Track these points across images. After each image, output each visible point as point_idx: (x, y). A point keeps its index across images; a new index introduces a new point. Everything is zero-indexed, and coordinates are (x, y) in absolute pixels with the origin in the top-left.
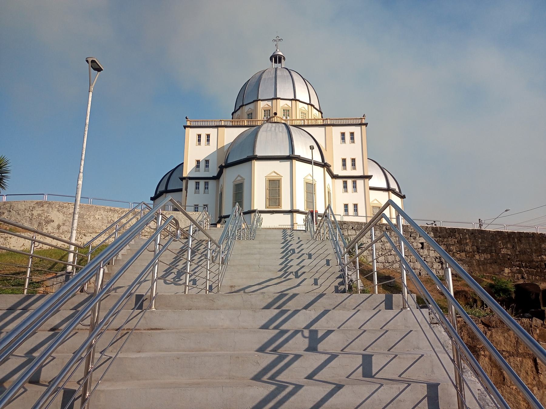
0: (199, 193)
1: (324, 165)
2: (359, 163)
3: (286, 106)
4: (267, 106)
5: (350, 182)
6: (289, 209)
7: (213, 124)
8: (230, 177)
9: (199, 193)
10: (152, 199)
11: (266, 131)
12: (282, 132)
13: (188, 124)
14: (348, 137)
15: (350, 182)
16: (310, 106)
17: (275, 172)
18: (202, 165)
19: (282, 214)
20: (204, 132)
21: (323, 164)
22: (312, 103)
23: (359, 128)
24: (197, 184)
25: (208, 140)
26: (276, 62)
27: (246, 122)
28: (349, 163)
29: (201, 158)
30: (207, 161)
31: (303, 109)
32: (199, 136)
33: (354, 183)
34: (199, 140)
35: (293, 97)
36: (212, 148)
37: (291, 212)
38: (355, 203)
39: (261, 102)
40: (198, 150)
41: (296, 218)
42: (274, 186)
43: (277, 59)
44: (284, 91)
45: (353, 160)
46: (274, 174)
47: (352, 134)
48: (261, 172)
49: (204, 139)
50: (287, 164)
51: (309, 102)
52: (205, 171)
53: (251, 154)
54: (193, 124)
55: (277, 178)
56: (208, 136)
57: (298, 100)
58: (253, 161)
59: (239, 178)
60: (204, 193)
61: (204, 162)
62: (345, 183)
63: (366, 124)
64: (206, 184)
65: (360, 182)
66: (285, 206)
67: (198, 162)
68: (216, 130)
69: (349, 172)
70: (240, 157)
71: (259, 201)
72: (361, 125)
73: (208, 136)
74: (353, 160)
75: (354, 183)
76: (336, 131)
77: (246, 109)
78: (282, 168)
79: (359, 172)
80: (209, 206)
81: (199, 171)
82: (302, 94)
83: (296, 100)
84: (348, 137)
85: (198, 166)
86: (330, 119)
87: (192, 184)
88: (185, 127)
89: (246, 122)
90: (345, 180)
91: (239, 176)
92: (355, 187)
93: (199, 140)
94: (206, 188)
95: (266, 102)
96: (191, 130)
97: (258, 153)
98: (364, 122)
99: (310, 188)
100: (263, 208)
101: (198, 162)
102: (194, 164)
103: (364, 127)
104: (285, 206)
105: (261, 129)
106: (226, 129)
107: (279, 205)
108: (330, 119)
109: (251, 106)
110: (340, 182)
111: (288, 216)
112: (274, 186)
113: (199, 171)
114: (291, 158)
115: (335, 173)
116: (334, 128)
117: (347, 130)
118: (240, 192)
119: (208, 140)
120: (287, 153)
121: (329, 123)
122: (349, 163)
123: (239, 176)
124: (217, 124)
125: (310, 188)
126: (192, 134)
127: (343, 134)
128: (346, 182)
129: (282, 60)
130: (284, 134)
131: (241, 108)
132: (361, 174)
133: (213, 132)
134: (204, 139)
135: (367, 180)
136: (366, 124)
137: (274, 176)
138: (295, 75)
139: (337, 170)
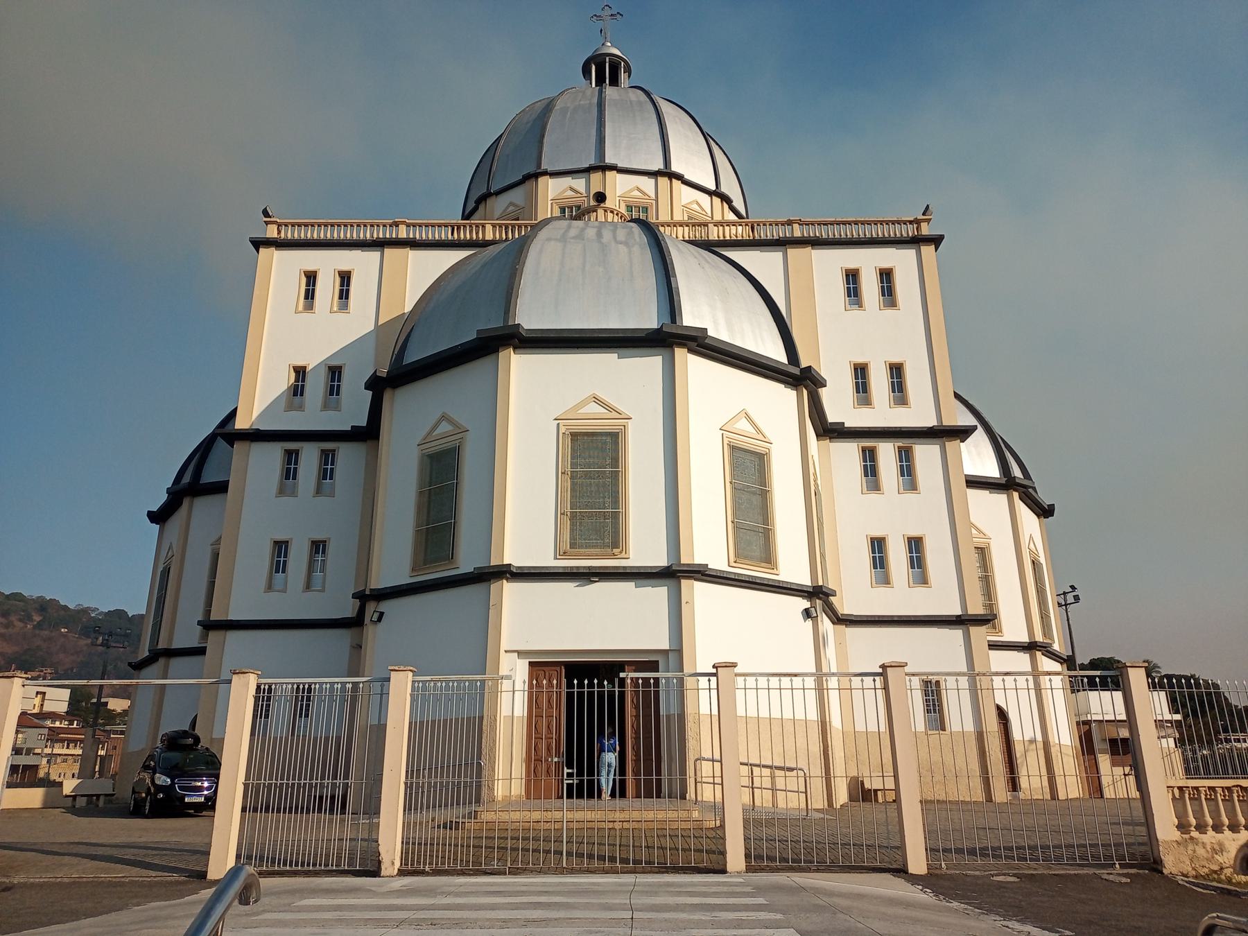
0: (293, 494)
1: (801, 378)
2: (917, 381)
3: (636, 193)
4: (570, 193)
5: (887, 452)
6: (660, 560)
7: (367, 235)
8: (413, 417)
9: (293, 494)
10: (154, 517)
11: (563, 239)
12: (626, 244)
13: (272, 232)
14: (870, 286)
15: (887, 452)
16: (717, 201)
17: (597, 400)
18: (316, 387)
19: (629, 586)
20: (327, 263)
21: (795, 371)
22: (724, 189)
23: (909, 254)
24: (291, 457)
25: (344, 295)
26: (600, 81)
27: (489, 228)
28: (879, 382)
29: (313, 358)
30: (335, 372)
31: (695, 207)
32: (311, 277)
33: (905, 457)
34: (310, 295)
35: (658, 165)
36: (359, 321)
37: (672, 574)
38: (914, 533)
39: (620, 177)
40: (300, 327)
41: (691, 603)
42: (593, 461)
43: (605, 70)
44: (630, 143)
45: (896, 370)
46: (594, 409)
47: (886, 276)
48: (536, 401)
49: (327, 288)
50: (650, 365)
51: (712, 186)
52: (326, 406)
53: (493, 323)
54: (289, 234)
55: (759, 446)
56: (345, 278)
57: (680, 177)
58: (502, 354)
59: (445, 427)
60: (318, 491)
61: (323, 373)
62: (869, 456)
63: (936, 241)
64: (327, 458)
65: (926, 455)
66: (644, 545)
67: (300, 372)
68: (374, 256)
69: (882, 414)
70: (462, 343)
71: (525, 515)
72: (916, 241)
73: (345, 278)
74: (896, 370)
75: (905, 457)
76: (827, 266)
77: (499, 205)
78: (629, 382)
79: (920, 415)
80: (331, 549)
81: (301, 408)
82: (691, 159)
83: (673, 176)
84: (870, 286)
85: (297, 390)
86: (801, 223)
87: (269, 457)
88: (258, 244)
89: (489, 228)
90: (868, 443)
91: (444, 417)
92: (907, 469)
93: (310, 295)
94: (326, 473)
95: (567, 181)
96: (278, 255)
97: (529, 318)
98: (926, 230)
99: (749, 469)
100: (547, 560)
101: (300, 372)
102: (285, 380)
103: (927, 250)
104: (644, 545)
105: (543, 234)
106: (413, 255)
107: (768, 558)
108: (801, 223)
109: (516, 196)
110: (850, 451)
111: (658, 594)
112: (593, 461)
113: (301, 408)
114: (668, 338)
115: (832, 417)
116: (818, 255)
117: (868, 261)
118: (449, 486)
119: (344, 295)
120: (649, 319)
121: (797, 234)
122: (879, 382)
123: (444, 417)
124: (380, 234)
125: (749, 469)
126: (282, 269)
127: (852, 277)
128: (297, 452)
129: (623, 76)
130: (636, 249)
131: (481, 207)
132: (931, 422)
133: (363, 264)
134: (327, 288)
135: (951, 445)
136: (936, 241)
137: (593, 418)
138: (665, 107)
139: (839, 405)
